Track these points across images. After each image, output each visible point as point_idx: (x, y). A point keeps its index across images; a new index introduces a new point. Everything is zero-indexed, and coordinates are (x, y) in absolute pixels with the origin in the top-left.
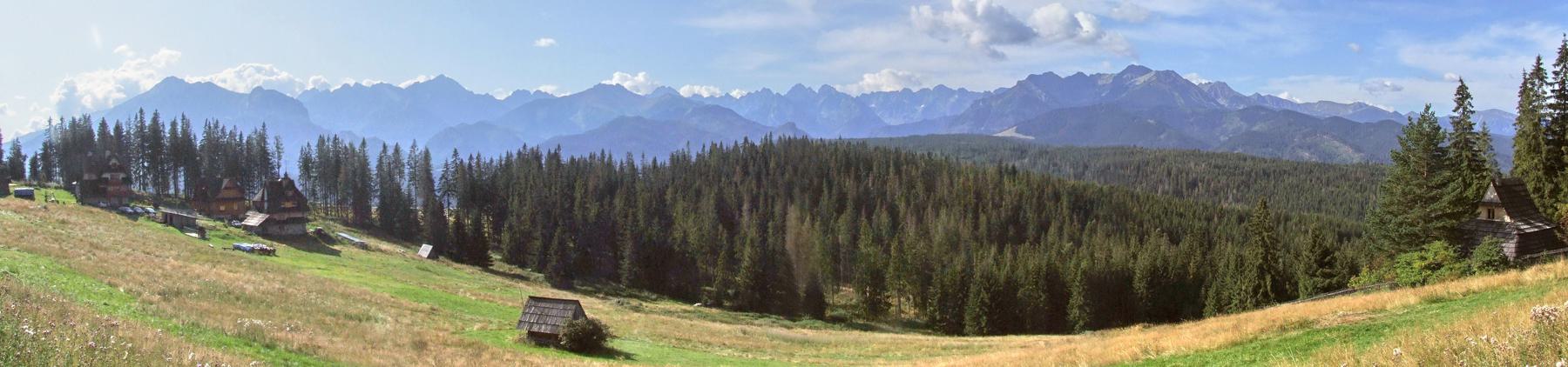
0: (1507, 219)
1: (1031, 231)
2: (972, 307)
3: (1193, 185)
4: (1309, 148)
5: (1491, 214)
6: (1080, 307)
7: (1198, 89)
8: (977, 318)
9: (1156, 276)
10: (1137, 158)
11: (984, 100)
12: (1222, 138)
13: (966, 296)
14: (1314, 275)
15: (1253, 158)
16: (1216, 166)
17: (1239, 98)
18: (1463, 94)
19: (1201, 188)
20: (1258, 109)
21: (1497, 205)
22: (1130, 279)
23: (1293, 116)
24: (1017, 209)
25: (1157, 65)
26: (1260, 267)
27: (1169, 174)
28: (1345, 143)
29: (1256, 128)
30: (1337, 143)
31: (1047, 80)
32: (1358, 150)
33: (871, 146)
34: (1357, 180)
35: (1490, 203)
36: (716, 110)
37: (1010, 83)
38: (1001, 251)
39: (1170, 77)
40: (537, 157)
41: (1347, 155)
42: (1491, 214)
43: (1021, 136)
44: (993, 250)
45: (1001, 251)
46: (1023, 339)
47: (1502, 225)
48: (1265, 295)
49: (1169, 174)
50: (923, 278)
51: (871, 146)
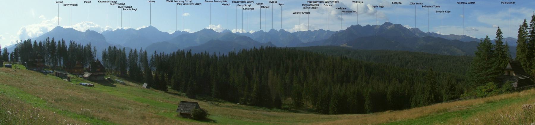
0: (514, 75)
3: (407, 63)
5: (509, 73)
7: (409, 30)
15: (428, 54)
17: (423, 33)
18: (499, 32)
21: (511, 70)
25: (395, 22)
26: (430, 91)
27: (399, 59)
29: (428, 44)
35: (508, 69)
36: (244, 37)
37: (344, 28)
38: (341, 85)
39: (399, 26)
42: (509, 73)
43: (348, 46)
44: (339, 85)
45: (341, 85)
47: (512, 76)
49: (399, 59)
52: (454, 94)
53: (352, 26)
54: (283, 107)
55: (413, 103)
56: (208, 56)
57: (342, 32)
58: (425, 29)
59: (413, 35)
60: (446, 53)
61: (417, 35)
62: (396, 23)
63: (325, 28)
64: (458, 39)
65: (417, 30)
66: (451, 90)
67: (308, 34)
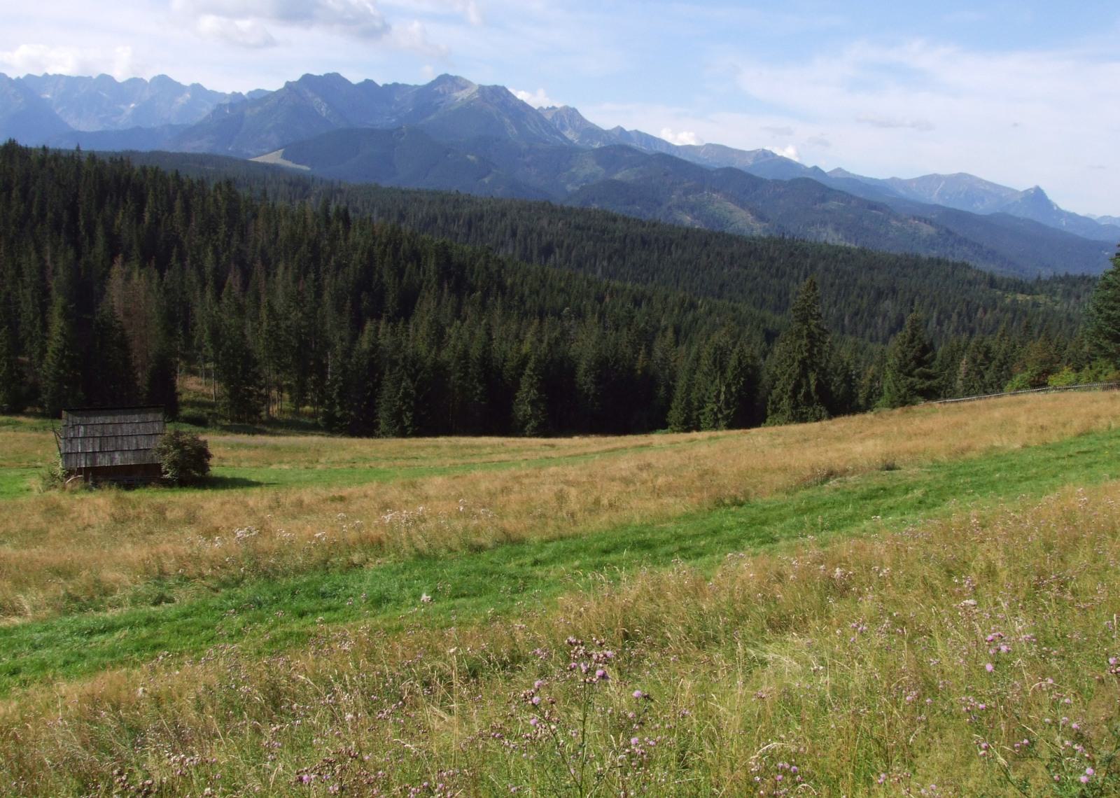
1: (391, 300)
2: (389, 396)
3: (547, 251)
4: (692, 209)
6: (533, 403)
8: (397, 416)
9: (604, 368)
10: (466, 211)
11: (232, 106)
12: (569, 188)
13: (378, 385)
14: (909, 374)
15: (625, 219)
16: (578, 227)
17: (593, 132)
19: (557, 256)
20: (622, 150)
22: (572, 371)
23: (671, 167)
24: (368, 270)
25: (480, 76)
26: (803, 362)
27: (514, 234)
28: (743, 206)
29: (618, 177)
30: (732, 207)
31: (330, 85)
32: (761, 218)
33: (137, 166)
34: (772, 260)
37: (274, 84)
38: (541, 321)
39: (498, 95)
40: (73, 156)
41: (743, 221)
43: (289, 164)
44: (536, 322)
45: (541, 321)
46: (454, 440)
48: (808, 395)
49: (514, 234)
50: (304, 357)
51: (137, 166)
52: (929, 377)
53: (307, 79)
54: (187, 411)
55: (675, 414)
56: (79, 166)
57: (259, 99)
58: (608, 115)
59: (550, 137)
60: (687, 220)
61: (570, 135)
62: (489, 81)
63: (185, 78)
64: (737, 165)
65: (571, 115)
66: (920, 363)
67: (98, 90)
